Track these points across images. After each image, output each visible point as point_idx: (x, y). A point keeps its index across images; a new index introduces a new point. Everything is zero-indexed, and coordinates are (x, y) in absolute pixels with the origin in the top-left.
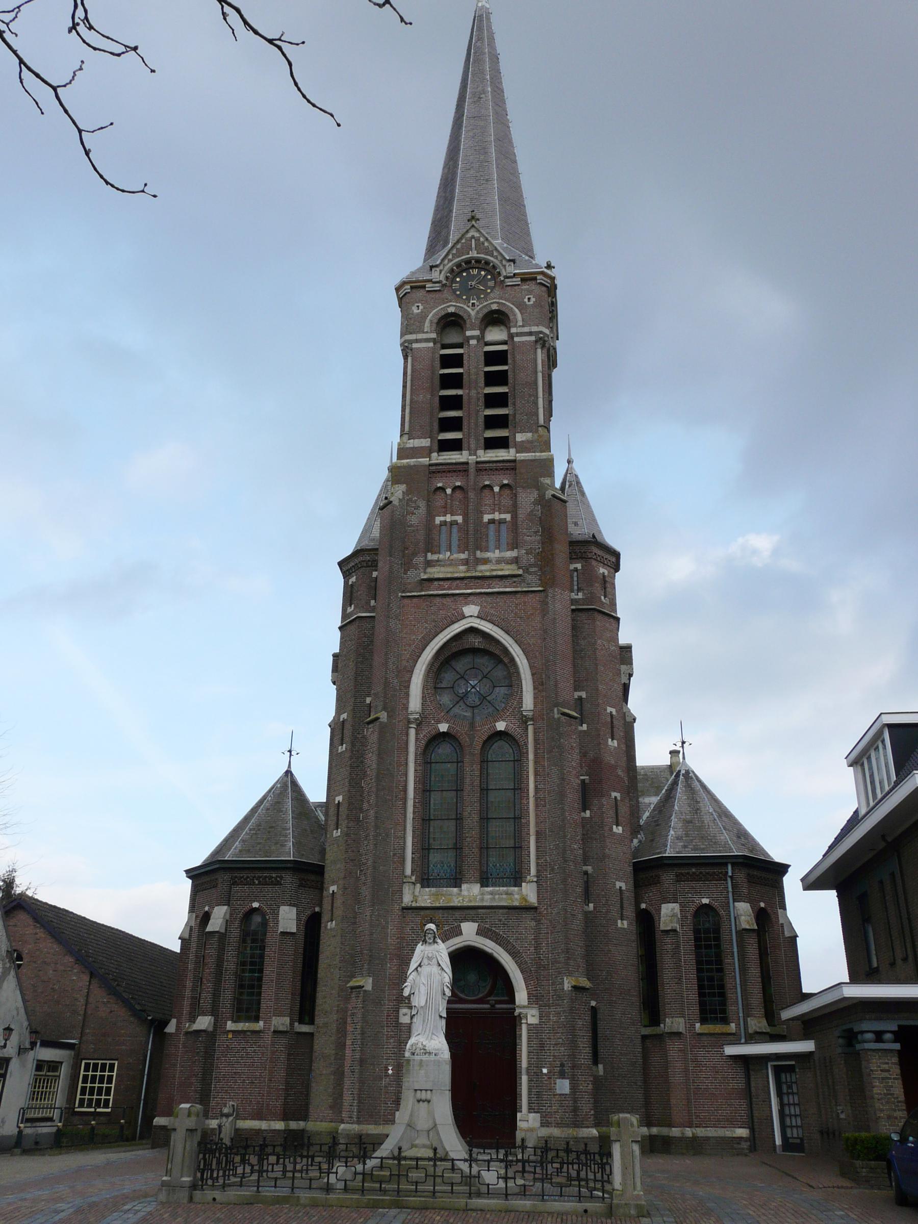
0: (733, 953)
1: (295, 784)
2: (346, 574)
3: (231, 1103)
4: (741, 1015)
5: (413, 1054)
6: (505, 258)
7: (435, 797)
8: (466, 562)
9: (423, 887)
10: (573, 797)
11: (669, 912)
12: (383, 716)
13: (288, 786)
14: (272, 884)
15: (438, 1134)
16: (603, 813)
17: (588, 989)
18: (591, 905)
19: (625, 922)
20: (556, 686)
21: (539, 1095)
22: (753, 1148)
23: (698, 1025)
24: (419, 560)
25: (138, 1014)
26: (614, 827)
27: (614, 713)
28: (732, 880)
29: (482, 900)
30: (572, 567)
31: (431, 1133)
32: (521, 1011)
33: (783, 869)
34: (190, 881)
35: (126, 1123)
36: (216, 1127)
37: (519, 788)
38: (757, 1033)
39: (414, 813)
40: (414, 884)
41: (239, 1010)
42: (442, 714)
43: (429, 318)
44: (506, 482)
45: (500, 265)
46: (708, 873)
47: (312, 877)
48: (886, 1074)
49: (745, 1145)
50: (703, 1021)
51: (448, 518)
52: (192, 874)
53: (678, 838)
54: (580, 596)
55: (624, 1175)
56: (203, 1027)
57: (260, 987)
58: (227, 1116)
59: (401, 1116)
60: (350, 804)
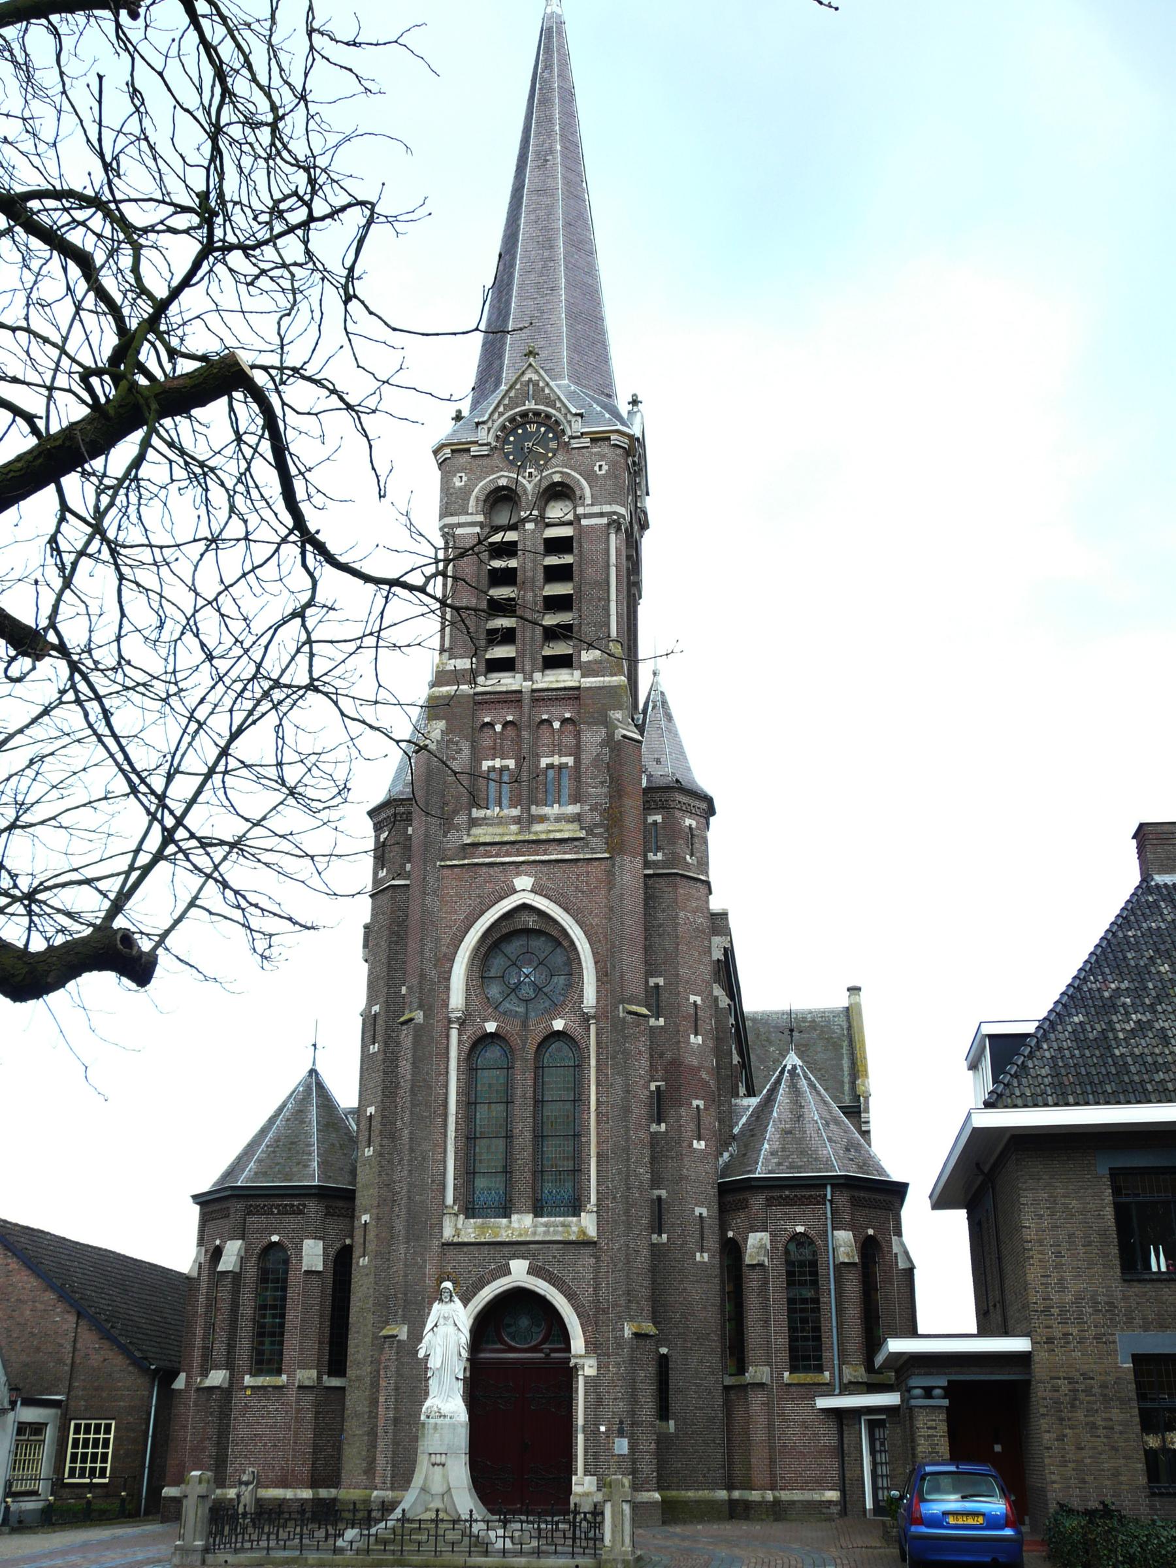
0: (829, 1290)
1: (320, 1086)
2: (378, 828)
3: (251, 1469)
4: (836, 1362)
5: (428, 1417)
6: (570, 412)
7: (482, 1112)
8: (517, 820)
9: (467, 1217)
10: (639, 1111)
11: (756, 1243)
12: (419, 1016)
13: (312, 1090)
14: (294, 1213)
15: (451, 1496)
16: (680, 1126)
17: (652, 1336)
18: (664, 1236)
19: (706, 1255)
20: (622, 977)
21: (596, 1457)
22: (844, 1512)
23: (786, 1374)
24: (461, 819)
25: (140, 1364)
26: (695, 1142)
27: (699, 1002)
28: (831, 1205)
29: (534, 1233)
30: (650, 819)
31: (445, 1496)
32: (577, 1361)
33: (899, 1191)
34: (197, 1208)
35: (127, 1495)
36: (235, 1497)
37: (579, 1099)
38: (851, 1383)
39: (456, 1130)
40: (456, 1215)
41: (259, 1362)
42: (490, 1010)
43: (474, 493)
44: (568, 715)
45: (564, 421)
46: (804, 1196)
47: (341, 1204)
48: (931, 1432)
49: (835, 1510)
50: (793, 1369)
51: (498, 763)
52: (202, 1200)
53: (773, 1153)
54: (660, 856)
55: (613, 1532)
56: (216, 1383)
57: (282, 1334)
58: (247, 1484)
59: (418, 1481)
60: (383, 1117)
